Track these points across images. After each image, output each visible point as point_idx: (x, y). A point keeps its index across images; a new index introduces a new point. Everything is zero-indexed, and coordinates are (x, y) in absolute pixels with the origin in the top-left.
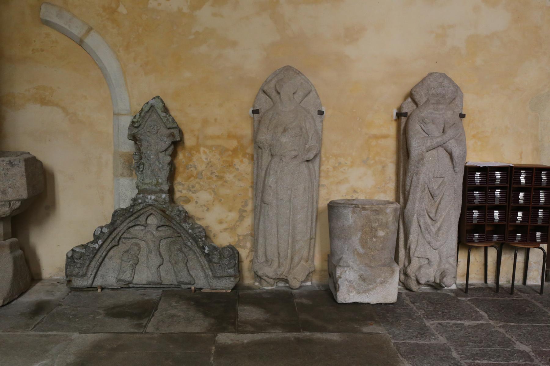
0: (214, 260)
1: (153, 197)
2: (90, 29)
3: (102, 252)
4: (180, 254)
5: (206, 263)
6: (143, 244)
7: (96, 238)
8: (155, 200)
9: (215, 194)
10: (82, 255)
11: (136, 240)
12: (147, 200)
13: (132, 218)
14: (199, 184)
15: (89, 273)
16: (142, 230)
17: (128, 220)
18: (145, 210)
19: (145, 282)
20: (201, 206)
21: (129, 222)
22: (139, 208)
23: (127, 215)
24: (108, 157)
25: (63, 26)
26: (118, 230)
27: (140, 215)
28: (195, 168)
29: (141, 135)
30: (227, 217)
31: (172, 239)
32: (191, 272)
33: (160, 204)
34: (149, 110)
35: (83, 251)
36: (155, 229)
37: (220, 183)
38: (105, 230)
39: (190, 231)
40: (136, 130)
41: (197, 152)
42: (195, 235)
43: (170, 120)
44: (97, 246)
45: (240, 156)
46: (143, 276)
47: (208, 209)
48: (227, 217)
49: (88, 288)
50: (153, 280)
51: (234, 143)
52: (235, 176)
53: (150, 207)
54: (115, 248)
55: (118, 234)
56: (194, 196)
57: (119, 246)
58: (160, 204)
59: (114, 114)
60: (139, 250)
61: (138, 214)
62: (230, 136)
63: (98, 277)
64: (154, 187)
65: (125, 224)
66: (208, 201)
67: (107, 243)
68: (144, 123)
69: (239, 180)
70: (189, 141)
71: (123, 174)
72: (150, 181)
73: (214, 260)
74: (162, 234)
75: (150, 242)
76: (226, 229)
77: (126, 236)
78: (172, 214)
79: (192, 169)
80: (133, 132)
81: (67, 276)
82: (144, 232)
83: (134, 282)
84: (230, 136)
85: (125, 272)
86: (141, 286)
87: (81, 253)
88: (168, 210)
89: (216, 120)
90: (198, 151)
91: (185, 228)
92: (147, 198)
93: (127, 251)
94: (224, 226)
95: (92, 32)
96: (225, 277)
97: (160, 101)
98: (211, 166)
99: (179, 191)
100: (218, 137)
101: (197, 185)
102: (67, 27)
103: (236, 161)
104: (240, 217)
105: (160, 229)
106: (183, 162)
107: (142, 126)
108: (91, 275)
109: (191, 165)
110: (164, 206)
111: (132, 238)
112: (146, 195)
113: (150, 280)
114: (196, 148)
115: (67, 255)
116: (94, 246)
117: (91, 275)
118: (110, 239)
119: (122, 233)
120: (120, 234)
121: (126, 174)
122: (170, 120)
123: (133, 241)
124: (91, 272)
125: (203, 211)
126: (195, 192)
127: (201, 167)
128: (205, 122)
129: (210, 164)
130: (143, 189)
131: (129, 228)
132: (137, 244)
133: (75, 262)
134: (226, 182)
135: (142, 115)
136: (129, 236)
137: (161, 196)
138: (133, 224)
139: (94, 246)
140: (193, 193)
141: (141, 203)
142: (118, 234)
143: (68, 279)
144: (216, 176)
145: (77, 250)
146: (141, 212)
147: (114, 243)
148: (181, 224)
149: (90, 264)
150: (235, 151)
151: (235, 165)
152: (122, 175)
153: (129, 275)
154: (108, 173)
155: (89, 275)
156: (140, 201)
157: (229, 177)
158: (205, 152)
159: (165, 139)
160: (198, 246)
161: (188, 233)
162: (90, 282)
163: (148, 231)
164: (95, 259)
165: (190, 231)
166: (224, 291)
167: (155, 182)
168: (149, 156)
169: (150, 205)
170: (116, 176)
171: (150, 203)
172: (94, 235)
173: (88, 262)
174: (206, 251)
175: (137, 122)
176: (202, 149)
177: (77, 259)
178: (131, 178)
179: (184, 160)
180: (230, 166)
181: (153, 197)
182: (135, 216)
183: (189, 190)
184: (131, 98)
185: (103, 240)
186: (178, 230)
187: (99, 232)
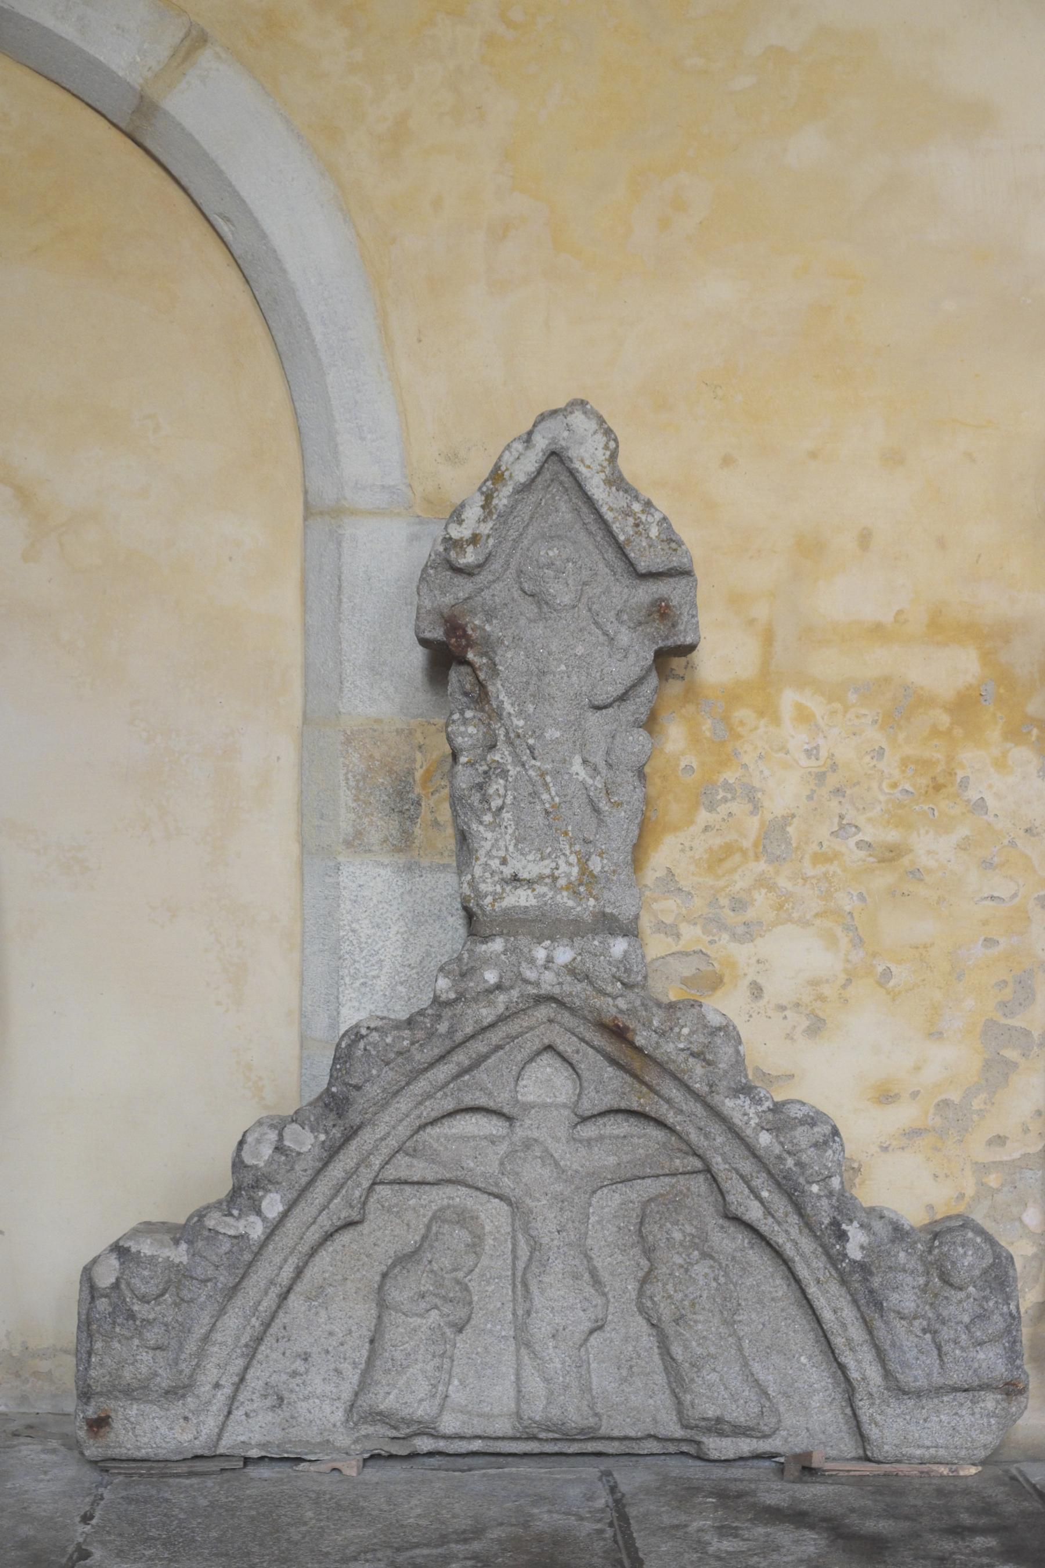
0: (894, 1297)
1: (564, 955)
2: (196, 40)
3: (278, 1260)
4: (701, 1269)
5: (849, 1313)
6: (493, 1216)
7: (245, 1187)
8: (571, 970)
9: (858, 942)
10: (178, 1278)
11: (459, 1196)
12: (530, 974)
13: (443, 1072)
14: (771, 888)
15: (211, 1373)
16: (493, 1141)
17: (422, 1085)
18: (513, 1027)
19: (503, 1426)
20: (782, 1008)
21: (429, 1096)
22: (487, 1014)
23: (422, 1057)
24: (270, 751)
25: (50, 22)
26: (367, 1138)
27: (485, 1057)
28: (752, 799)
29: (490, 615)
30: (918, 1068)
31: (650, 1187)
32: (756, 1367)
33: (602, 993)
34: (554, 476)
35: (180, 1254)
36: (562, 1133)
37: (883, 880)
38: (304, 1141)
39: (765, 1139)
40: (463, 588)
41: (761, 714)
42: (790, 1162)
43: (654, 532)
44: (256, 1230)
45: (994, 734)
46: (481, 1390)
47: (816, 1027)
48: (918, 1068)
49: (197, 1457)
50: (555, 1412)
51: (953, 669)
52: (964, 846)
53: (544, 1012)
54: (345, 1238)
55: (364, 1161)
56: (742, 953)
57: (365, 1228)
58: (602, 993)
59: (309, 512)
60: (475, 1246)
61: (479, 1047)
62: (941, 628)
63: (251, 1398)
64: (565, 899)
65: (403, 1104)
66: (814, 983)
67: (305, 1211)
68: (507, 546)
69: (987, 865)
70: (722, 654)
71: (359, 834)
72: (545, 868)
73: (894, 1297)
74: (606, 1159)
75: (539, 1204)
76: (913, 1133)
77: (403, 1174)
78: (670, 1047)
79: (734, 807)
80: (448, 599)
81: (85, 1395)
82: (503, 1148)
83: (449, 1424)
84: (941, 628)
85: (404, 1368)
86: (477, 1445)
87: (170, 1265)
88: (647, 1025)
89: (865, 539)
90: (769, 711)
91: (737, 1119)
92: (532, 961)
93: (406, 1259)
94: (904, 1115)
95: (206, 58)
96: (955, 1389)
97: (593, 425)
98: (838, 791)
99: (662, 927)
100: (878, 632)
101: (760, 897)
102: (67, 30)
103: (972, 758)
104: (988, 1065)
105: (589, 1131)
106: (689, 769)
107: (496, 565)
108: (217, 1386)
109: (727, 787)
110: (622, 1003)
111: (437, 1183)
112: (523, 941)
113: (536, 1410)
114: (761, 690)
115: (87, 1274)
116: (239, 1227)
117: (217, 1386)
118: (322, 1189)
119: (385, 1151)
120: (376, 1162)
121: (374, 837)
122: (654, 532)
123: (439, 1197)
124: (217, 1368)
125: (789, 1037)
126: (749, 933)
127: (785, 792)
128: (810, 549)
129: (827, 779)
130: (506, 911)
131: (422, 1127)
132: (464, 1218)
133: (131, 1316)
134: (916, 874)
135: (502, 500)
136: (420, 1169)
137: (605, 952)
138: (449, 1105)
139: (239, 1227)
140: (734, 937)
141: (499, 987)
142: (364, 1161)
143: (91, 1412)
144: (859, 845)
145: (146, 1248)
146: (495, 1037)
147: (340, 1211)
148: (716, 1099)
149: (213, 1328)
150: (966, 706)
151: (964, 784)
152: (355, 842)
153: (422, 1388)
154: (270, 841)
155: (205, 1389)
156: (491, 977)
157: (932, 848)
158: (804, 716)
159: (625, 637)
160: (808, 1225)
161: (752, 1152)
162: (210, 1424)
163: (528, 1144)
164: (239, 1300)
165: (765, 1139)
166: (944, 1470)
167: (568, 869)
168: (538, 732)
169: (550, 998)
170: (315, 852)
171: (546, 989)
172: (238, 1164)
173: (206, 1320)
174: (854, 1251)
175: (475, 539)
176: (789, 699)
177: (144, 1299)
178: (401, 859)
179: (690, 759)
180: (938, 788)
181: (564, 955)
182: (461, 1058)
183: (714, 923)
184: (418, 427)
185: (291, 1195)
186: (694, 1137)
187: (267, 1151)
